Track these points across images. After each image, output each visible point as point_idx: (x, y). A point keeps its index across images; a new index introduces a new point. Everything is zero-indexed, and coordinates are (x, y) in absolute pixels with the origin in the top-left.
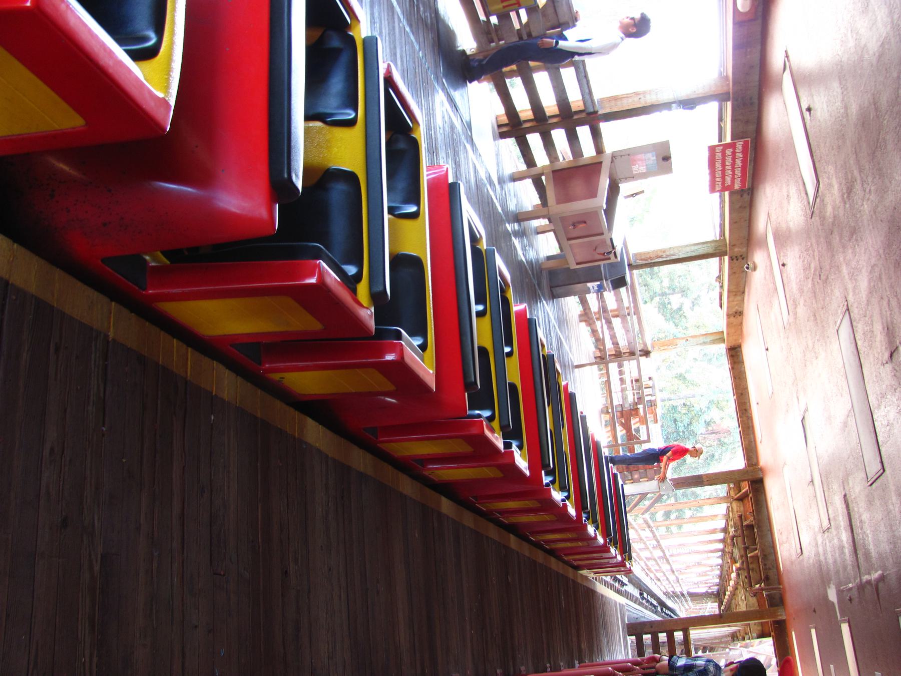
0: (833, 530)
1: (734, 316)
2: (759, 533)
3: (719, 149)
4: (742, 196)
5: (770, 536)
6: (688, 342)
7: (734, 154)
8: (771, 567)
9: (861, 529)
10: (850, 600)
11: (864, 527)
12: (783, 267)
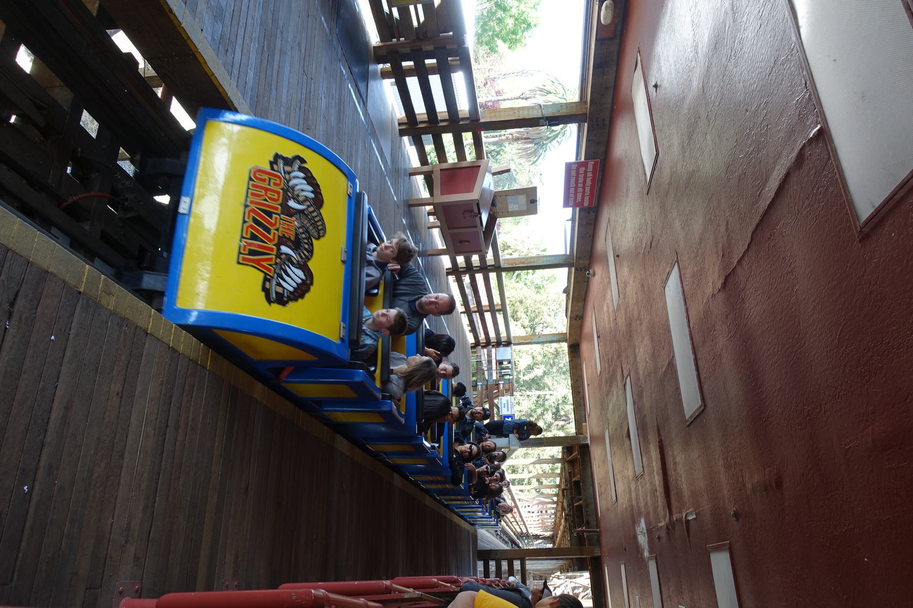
0: (647, 477)
1: (576, 319)
3: (574, 167)
4: (589, 213)
5: (591, 489)
7: (586, 172)
9: (675, 470)
10: (659, 538)
11: (677, 468)
12: (617, 258)
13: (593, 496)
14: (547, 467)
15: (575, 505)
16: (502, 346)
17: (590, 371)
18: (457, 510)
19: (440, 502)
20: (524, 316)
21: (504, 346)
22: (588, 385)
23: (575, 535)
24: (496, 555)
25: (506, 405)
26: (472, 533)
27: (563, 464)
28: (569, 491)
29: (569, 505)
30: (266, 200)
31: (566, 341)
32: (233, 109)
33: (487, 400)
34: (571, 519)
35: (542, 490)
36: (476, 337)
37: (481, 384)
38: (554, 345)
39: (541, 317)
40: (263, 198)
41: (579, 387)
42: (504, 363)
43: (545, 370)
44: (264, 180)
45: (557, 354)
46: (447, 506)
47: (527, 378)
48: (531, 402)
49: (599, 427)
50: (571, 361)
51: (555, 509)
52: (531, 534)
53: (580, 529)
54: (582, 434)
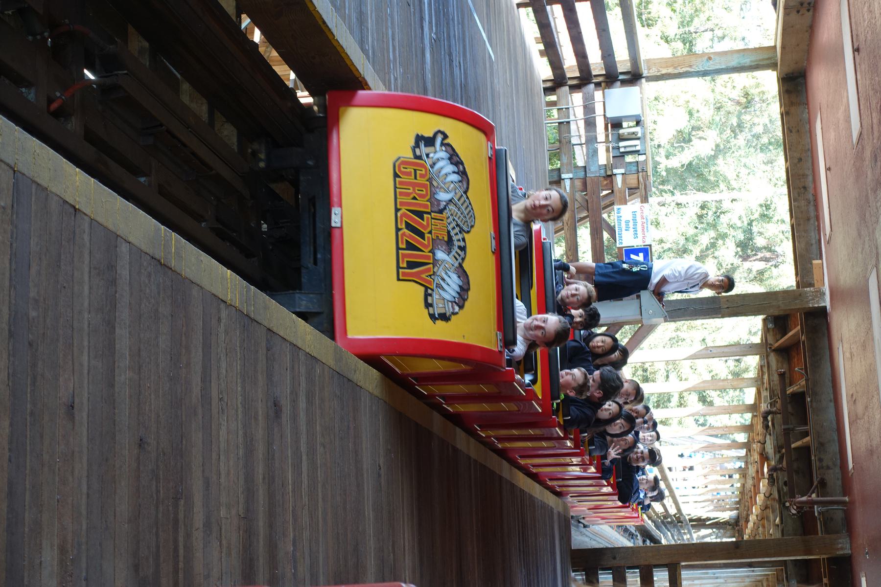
1: (798, 12)
2: (814, 404)
6: (711, 62)
8: (830, 464)
13: (835, 426)
14: (722, 368)
15: (793, 446)
16: (619, 83)
17: (833, 134)
18: (522, 462)
19: (485, 443)
20: (666, 12)
21: (624, 83)
22: (828, 169)
23: (794, 512)
24: (614, 558)
25: (631, 224)
26: (559, 513)
27: (765, 357)
28: (779, 416)
29: (778, 449)
30: (414, 198)
31: (773, 66)
32: (365, 87)
33: (584, 214)
34: (783, 477)
35: (711, 420)
36: (556, 63)
37: (571, 176)
38: (743, 79)
39: (707, 14)
40: (412, 196)
41: (804, 176)
42: (625, 124)
43: (718, 141)
44: (409, 174)
45: (747, 102)
46: (503, 454)
47: (675, 162)
48: (687, 219)
49: (853, 266)
50: (785, 115)
51: (746, 459)
52: (687, 518)
53: (804, 498)
54: (811, 285)
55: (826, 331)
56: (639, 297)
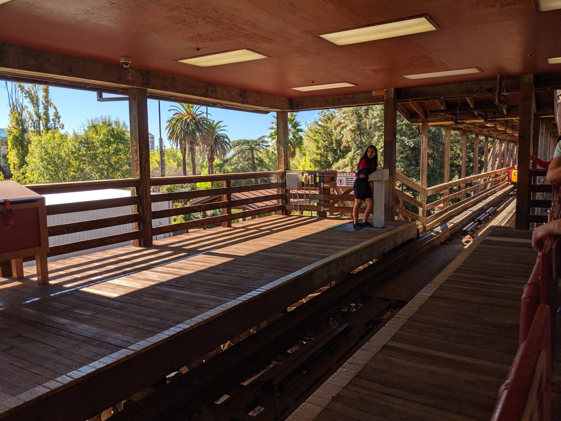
6: (281, 141)
15: (467, 98)
55: (9, 4)
56: (372, 182)
